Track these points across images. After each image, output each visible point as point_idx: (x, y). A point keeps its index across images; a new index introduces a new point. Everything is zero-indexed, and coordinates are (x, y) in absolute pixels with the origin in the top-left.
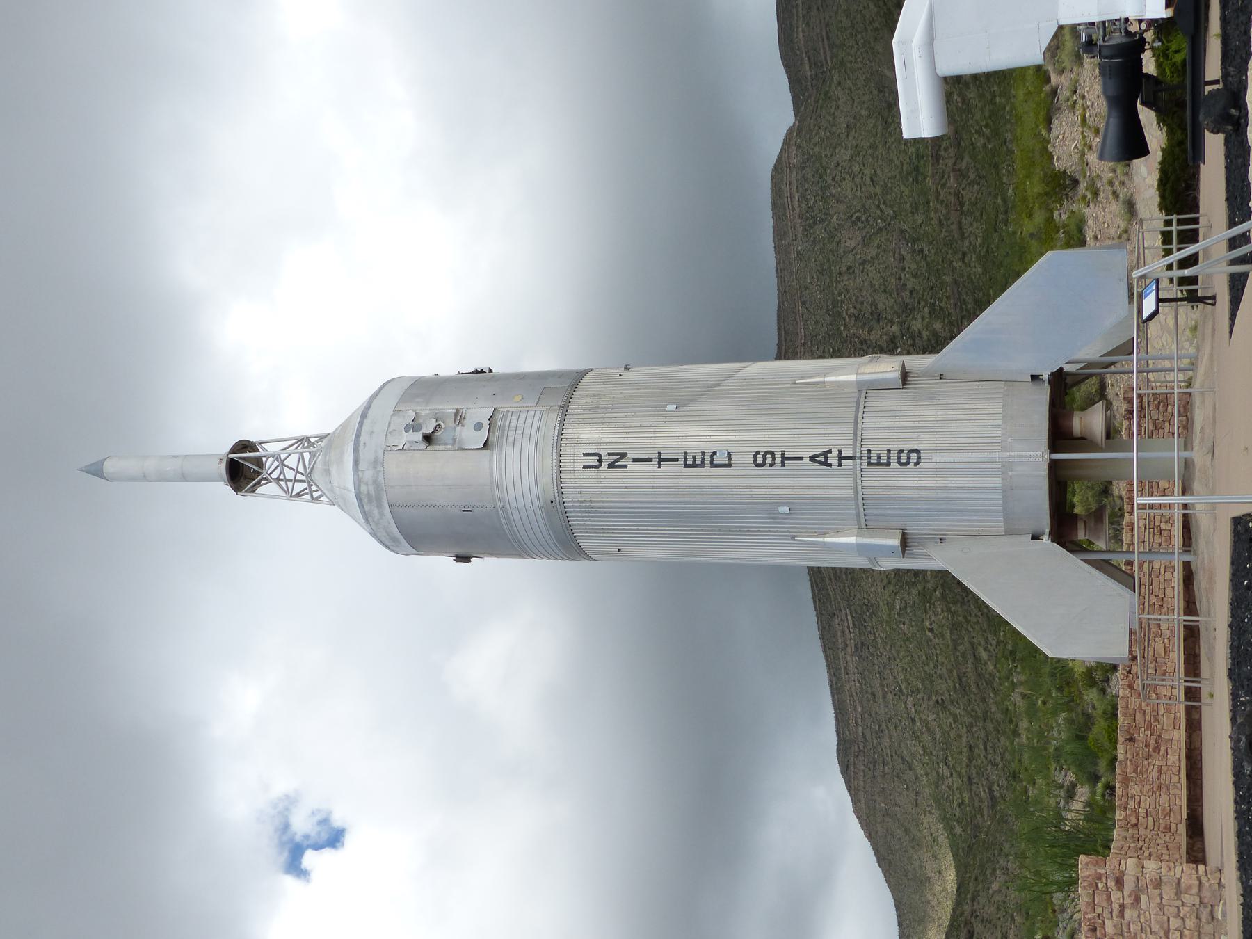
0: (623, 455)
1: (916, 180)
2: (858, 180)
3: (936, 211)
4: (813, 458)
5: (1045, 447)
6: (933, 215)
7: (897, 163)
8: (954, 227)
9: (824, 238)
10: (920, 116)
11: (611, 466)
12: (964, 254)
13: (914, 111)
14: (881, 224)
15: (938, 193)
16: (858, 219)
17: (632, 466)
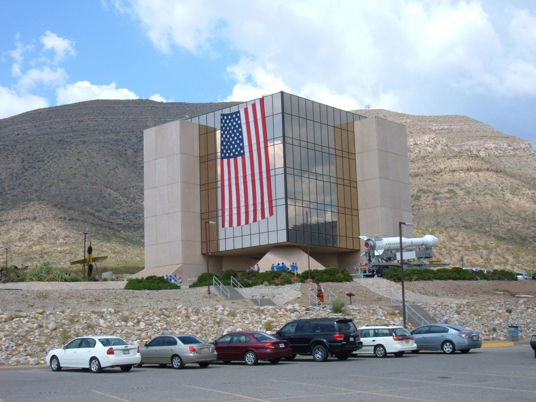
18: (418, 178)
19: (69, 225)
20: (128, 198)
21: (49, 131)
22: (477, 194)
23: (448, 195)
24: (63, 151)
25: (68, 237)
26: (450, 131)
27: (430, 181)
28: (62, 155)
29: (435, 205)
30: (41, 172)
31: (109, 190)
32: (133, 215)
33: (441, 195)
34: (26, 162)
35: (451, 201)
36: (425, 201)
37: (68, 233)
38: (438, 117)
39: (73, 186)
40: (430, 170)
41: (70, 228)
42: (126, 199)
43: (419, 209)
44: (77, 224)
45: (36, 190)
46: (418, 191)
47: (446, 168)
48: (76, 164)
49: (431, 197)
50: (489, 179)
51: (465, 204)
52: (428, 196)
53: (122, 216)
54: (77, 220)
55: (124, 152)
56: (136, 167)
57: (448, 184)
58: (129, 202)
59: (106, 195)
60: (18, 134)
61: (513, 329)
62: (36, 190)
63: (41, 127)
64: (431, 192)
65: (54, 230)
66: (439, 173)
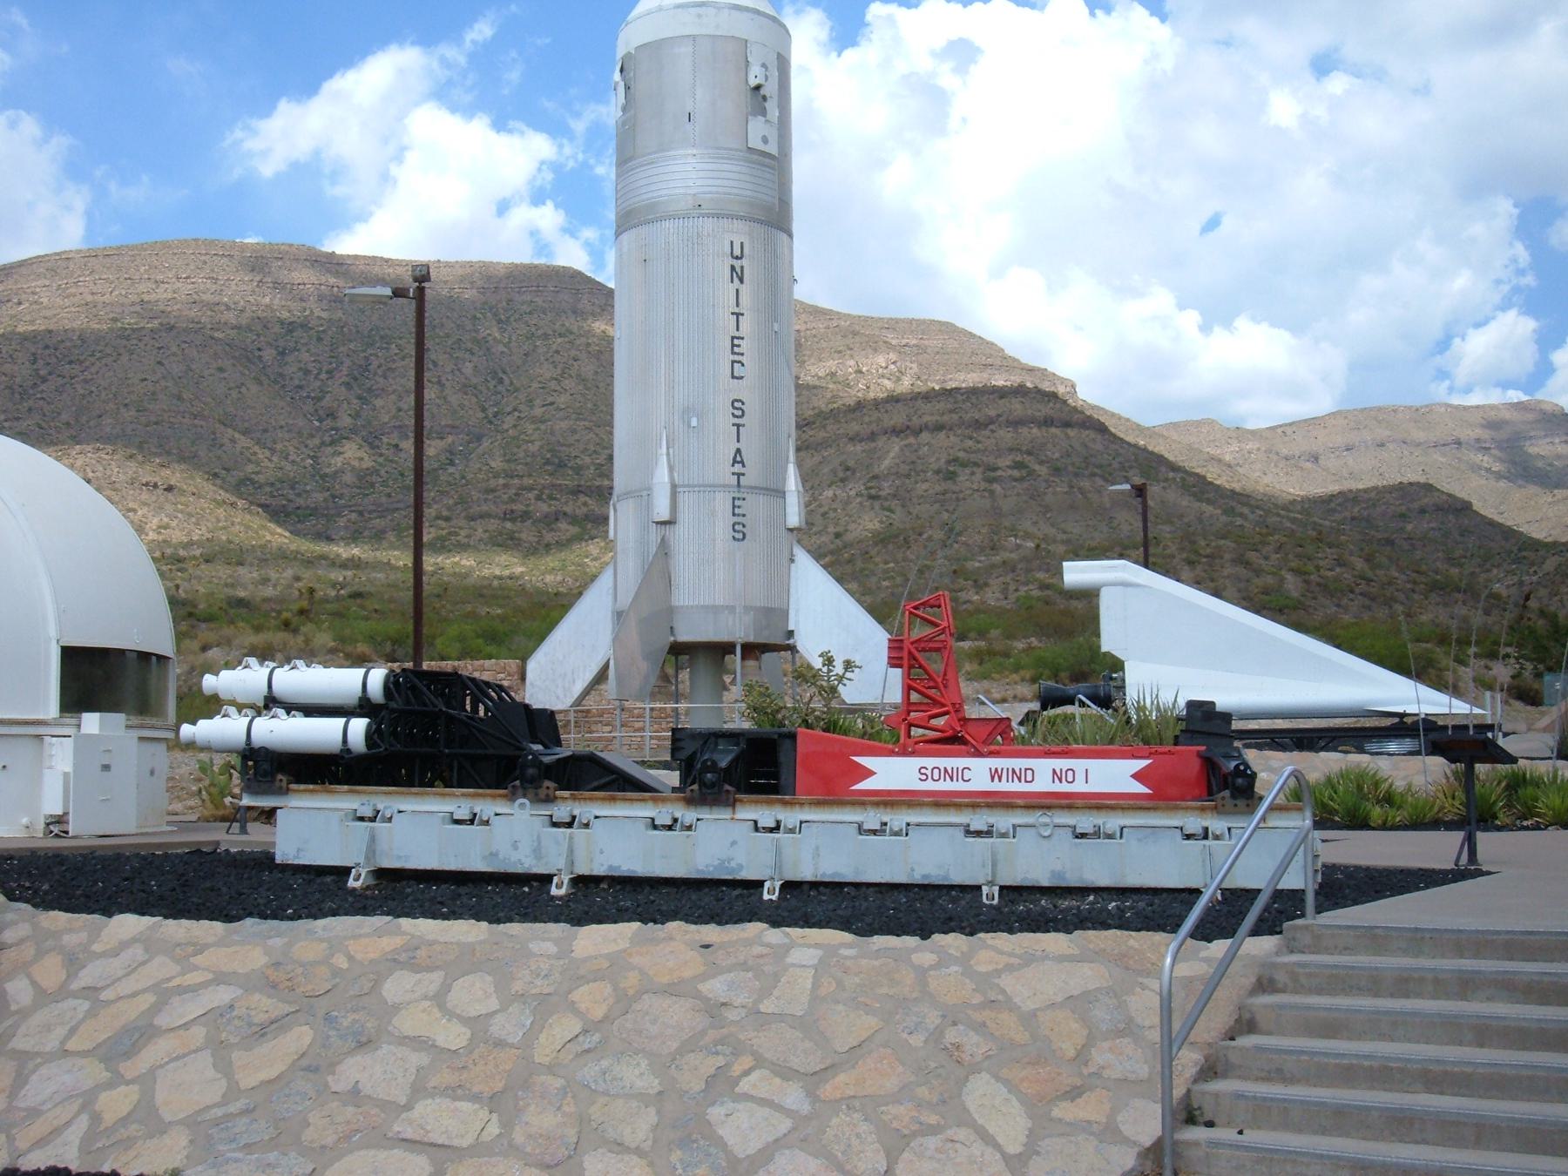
0: (741, 281)
1: (548, 462)
2: (553, 384)
3: (506, 486)
4: (738, 451)
5: (746, 640)
6: (501, 481)
7: (571, 440)
8: (485, 508)
9: (477, 331)
10: (1077, 573)
11: (733, 268)
12: (447, 519)
13: (1083, 571)
14: (490, 412)
15: (531, 489)
16: (501, 381)
17: (732, 288)
18: (942, 435)
19: (167, 500)
20: (273, 451)
21: (89, 298)
22: (1076, 475)
23: (1016, 473)
24: (124, 342)
25: (166, 527)
26: (921, 350)
27: (970, 443)
28: (122, 351)
29: (992, 492)
30: (78, 386)
31: (230, 431)
32: (293, 488)
33: (999, 473)
34: (41, 363)
35: (1026, 485)
36: (968, 484)
37: (166, 520)
38: (897, 321)
39: (153, 419)
40: (967, 417)
41: (169, 508)
42: (268, 453)
43: (958, 499)
44: (183, 499)
45: (68, 424)
46: (949, 462)
47: (999, 416)
48: (154, 372)
49: (979, 476)
50: (1091, 445)
51: (1054, 493)
52: (973, 473)
53: (268, 489)
54: (182, 492)
55: (257, 353)
56: (283, 386)
57: (1011, 450)
58: (275, 459)
59: (226, 441)
60: (20, 303)
61: (364, 1039)
62: (68, 424)
63: (73, 290)
64: (976, 464)
65: (134, 511)
66: (986, 426)
